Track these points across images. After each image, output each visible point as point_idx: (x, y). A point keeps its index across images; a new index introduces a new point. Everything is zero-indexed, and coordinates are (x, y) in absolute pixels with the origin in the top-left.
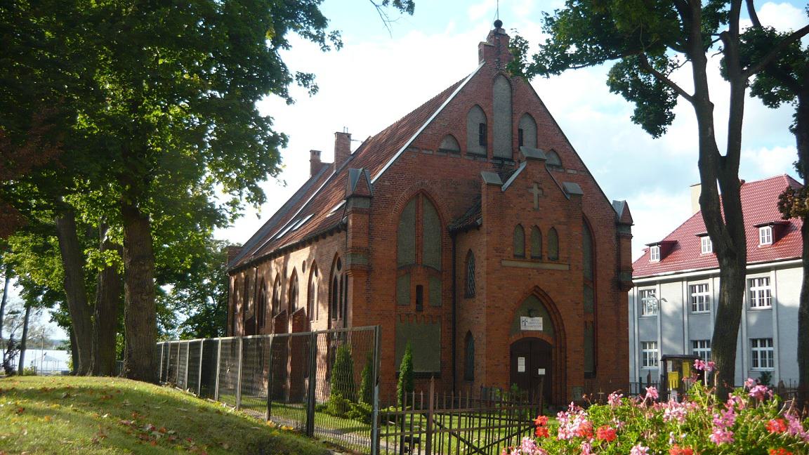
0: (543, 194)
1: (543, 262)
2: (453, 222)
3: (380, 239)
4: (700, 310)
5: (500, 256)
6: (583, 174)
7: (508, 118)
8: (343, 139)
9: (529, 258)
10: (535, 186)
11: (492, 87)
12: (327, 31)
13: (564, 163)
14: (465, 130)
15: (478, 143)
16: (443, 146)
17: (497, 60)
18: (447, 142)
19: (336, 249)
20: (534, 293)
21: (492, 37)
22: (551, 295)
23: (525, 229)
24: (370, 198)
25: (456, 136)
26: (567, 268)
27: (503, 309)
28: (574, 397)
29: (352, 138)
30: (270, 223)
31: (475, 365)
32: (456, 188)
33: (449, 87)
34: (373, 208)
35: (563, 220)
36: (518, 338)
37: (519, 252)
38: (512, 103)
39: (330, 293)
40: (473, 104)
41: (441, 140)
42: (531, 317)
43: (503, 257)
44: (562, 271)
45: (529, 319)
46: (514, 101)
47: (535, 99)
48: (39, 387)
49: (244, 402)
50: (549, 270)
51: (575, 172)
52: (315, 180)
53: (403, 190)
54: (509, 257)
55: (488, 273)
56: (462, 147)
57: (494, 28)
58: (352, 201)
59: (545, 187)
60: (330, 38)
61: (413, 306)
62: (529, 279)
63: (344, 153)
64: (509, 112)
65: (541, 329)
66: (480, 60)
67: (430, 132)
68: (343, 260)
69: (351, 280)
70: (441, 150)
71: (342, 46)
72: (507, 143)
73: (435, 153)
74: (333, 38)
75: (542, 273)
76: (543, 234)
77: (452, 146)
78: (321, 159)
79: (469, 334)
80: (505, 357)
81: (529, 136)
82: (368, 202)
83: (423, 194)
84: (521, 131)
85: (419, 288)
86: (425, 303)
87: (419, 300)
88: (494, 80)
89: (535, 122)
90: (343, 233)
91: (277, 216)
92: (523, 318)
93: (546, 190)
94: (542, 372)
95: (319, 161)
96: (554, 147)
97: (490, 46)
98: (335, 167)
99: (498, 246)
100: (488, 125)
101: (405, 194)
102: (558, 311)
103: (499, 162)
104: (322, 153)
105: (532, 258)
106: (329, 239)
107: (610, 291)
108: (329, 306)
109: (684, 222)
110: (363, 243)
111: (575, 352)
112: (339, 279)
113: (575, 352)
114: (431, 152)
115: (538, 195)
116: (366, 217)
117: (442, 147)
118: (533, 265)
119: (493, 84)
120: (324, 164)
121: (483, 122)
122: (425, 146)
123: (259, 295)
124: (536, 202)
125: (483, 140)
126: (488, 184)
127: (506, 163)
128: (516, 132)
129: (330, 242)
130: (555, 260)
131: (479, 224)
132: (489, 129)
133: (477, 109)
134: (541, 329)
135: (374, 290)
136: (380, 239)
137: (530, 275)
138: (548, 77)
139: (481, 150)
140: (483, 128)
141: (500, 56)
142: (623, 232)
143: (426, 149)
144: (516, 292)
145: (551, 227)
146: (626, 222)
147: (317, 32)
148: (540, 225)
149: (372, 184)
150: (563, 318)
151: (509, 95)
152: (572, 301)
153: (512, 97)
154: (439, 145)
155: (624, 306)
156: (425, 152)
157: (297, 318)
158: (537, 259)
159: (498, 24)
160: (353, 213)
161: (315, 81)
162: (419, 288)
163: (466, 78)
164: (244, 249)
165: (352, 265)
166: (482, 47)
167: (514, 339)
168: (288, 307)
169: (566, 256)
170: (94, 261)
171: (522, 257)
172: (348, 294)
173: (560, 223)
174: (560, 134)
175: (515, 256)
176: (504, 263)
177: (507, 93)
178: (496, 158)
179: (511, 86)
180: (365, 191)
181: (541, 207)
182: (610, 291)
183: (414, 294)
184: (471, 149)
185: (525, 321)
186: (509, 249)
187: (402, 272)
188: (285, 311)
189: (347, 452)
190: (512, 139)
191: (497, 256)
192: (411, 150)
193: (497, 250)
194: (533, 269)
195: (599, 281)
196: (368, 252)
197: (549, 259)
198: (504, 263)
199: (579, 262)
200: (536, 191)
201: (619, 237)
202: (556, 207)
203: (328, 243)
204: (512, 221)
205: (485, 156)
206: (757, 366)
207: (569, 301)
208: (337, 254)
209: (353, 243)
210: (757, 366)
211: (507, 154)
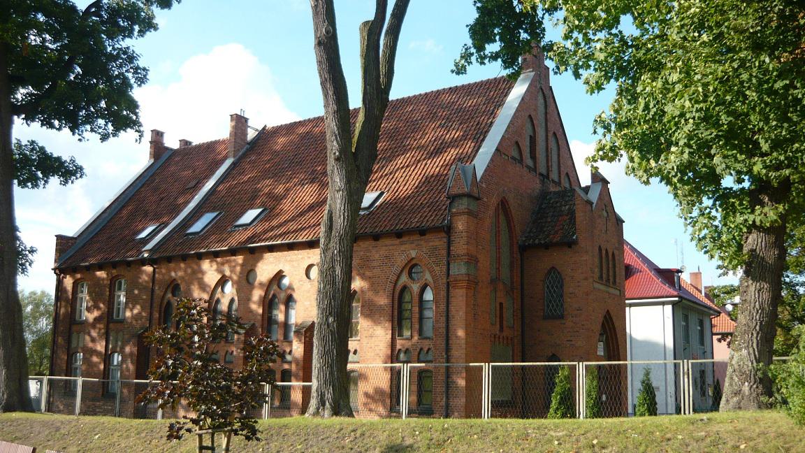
8: (240, 122)
30: (113, 206)
33: (288, 123)
48: (657, 399)
49: (672, 408)
63: (242, 140)
78: (165, 141)
91: (123, 196)
95: (162, 144)
104: (165, 136)
108: (392, 321)
120: (167, 149)
164: (78, 241)
168: (102, 373)
170: (631, 40)
206: (479, 415)
210: (479, 415)
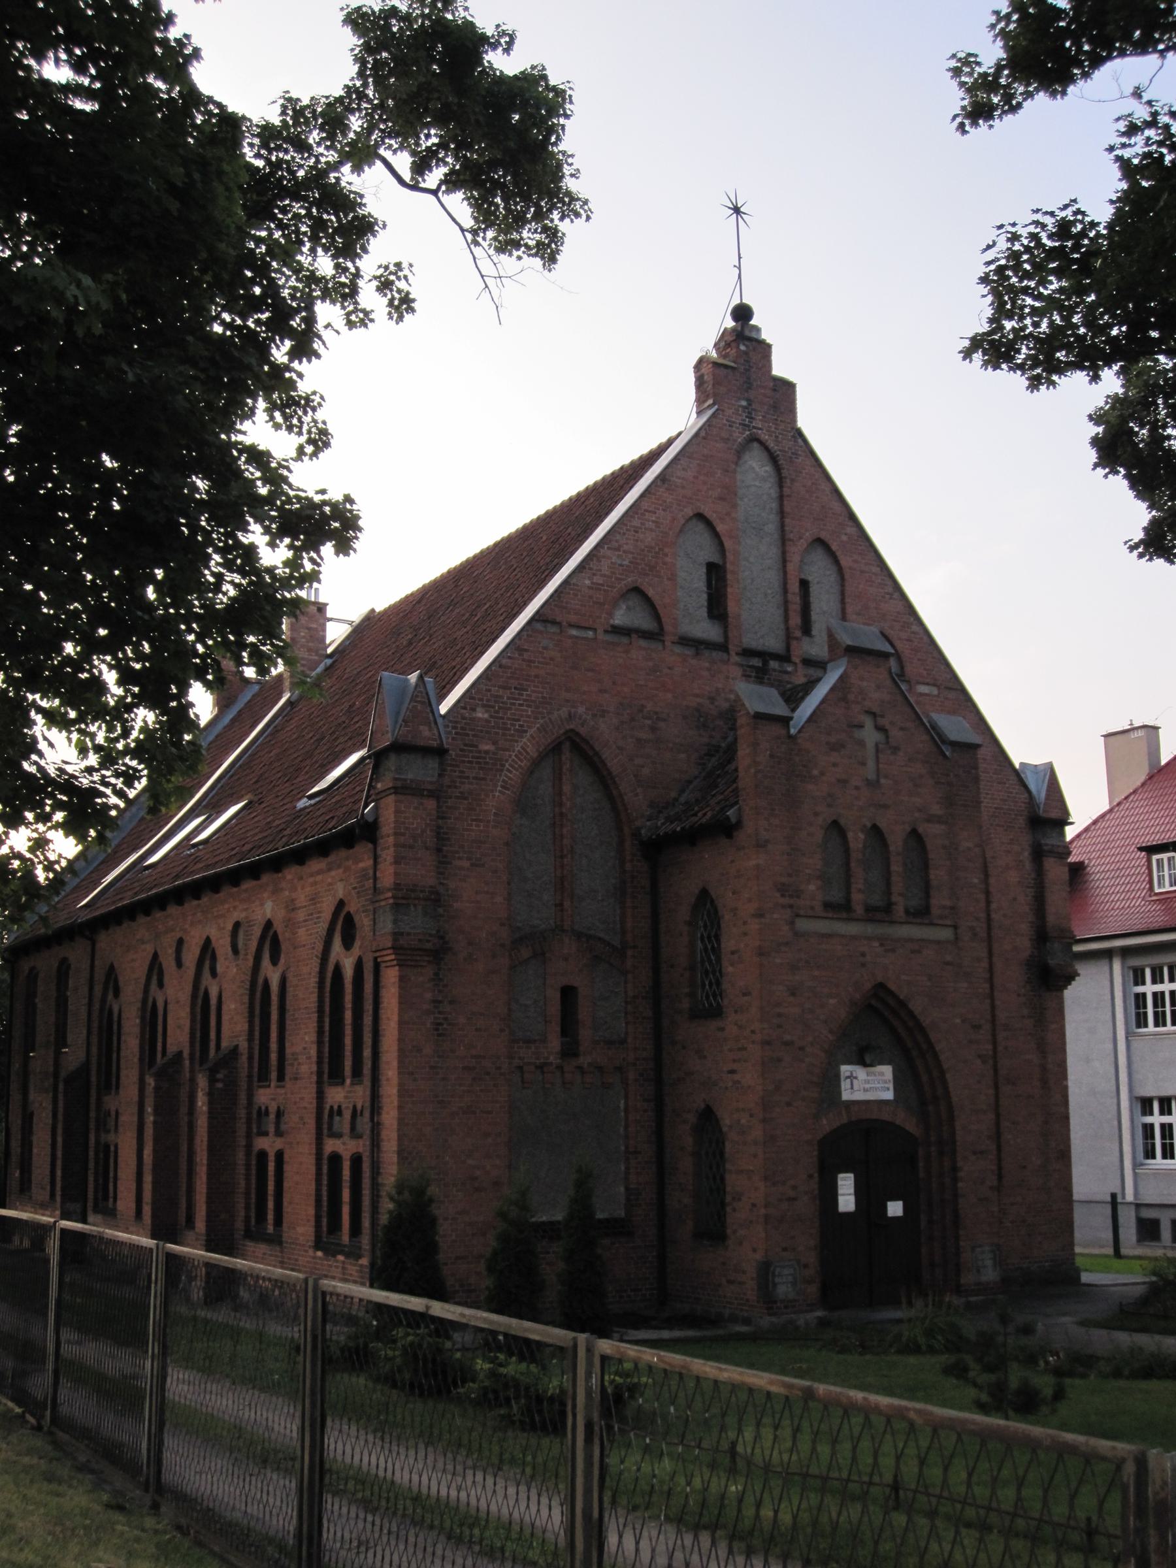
0: (888, 743)
1: (892, 922)
2: (650, 819)
3: (466, 864)
4: (1157, 1025)
5: (791, 906)
6: (952, 695)
7: (774, 552)
9: (859, 910)
10: (869, 723)
11: (735, 472)
12: (369, 264)
13: (908, 669)
14: (673, 578)
15: (704, 612)
16: (620, 617)
17: (744, 403)
18: (628, 608)
19: (340, 891)
20: (873, 1002)
21: (728, 345)
22: (916, 1006)
23: (850, 835)
24: (440, 752)
25: (650, 593)
26: (945, 934)
27: (802, 1049)
28: (978, 1271)
29: (329, 614)
31: (728, 1199)
32: (653, 729)
34: (446, 781)
35: (936, 810)
36: (837, 1124)
37: (837, 896)
38: (782, 513)
39: (320, 1011)
40: (689, 512)
41: (615, 604)
42: (864, 1064)
44: (938, 942)
45: (860, 1072)
46: (787, 509)
47: (836, 506)
50: (911, 940)
51: (935, 691)
52: (226, 720)
53: (522, 732)
54: (812, 908)
55: (761, 952)
56: (668, 628)
57: (730, 323)
58: (392, 762)
59: (892, 723)
60: (375, 283)
61: (555, 1043)
62: (863, 965)
63: (310, 650)
64: (776, 536)
65: (889, 1095)
66: (700, 400)
67: (587, 582)
68: (363, 922)
69: (391, 976)
70: (616, 630)
71: (411, 310)
72: (773, 613)
73: (601, 636)
74: (385, 285)
75: (893, 950)
76: (892, 848)
77: (640, 619)
79: (708, 1116)
80: (811, 1176)
81: (824, 603)
82: (433, 764)
83: (573, 743)
84: (804, 584)
86: (585, 1034)
87: (568, 1024)
88: (740, 453)
89: (836, 561)
90: (363, 850)
92: (845, 1069)
93: (894, 733)
94: (895, 1209)
97: (726, 367)
98: (287, 684)
100: (728, 566)
101: (527, 745)
102: (931, 1046)
103: (756, 662)
106: (316, 864)
109: (1094, 818)
110: (422, 873)
112: (348, 972)
113: (975, 1153)
114: (590, 634)
115: (877, 745)
116: (431, 804)
118: (870, 929)
119: (736, 464)
121: (715, 558)
122: (573, 618)
123: (102, 1010)
124: (871, 764)
125: (717, 607)
126: (759, 716)
127: (773, 664)
128: (794, 587)
129: (319, 872)
130: (921, 914)
131: (733, 820)
132: (729, 576)
133: (700, 527)
134: (889, 1095)
135: (451, 1002)
136: (466, 864)
137: (863, 955)
138: (1053, 383)
139: (707, 630)
140: (716, 574)
142: (1049, 841)
143: (579, 627)
144: (832, 1001)
145: (908, 829)
146: (1054, 814)
147: (337, 266)
148: (883, 824)
149: (443, 717)
150: (945, 1066)
151: (774, 493)
152: (963, 1021)
153: (781, 497)
154: (611, 615)
155: (1054, 1026)
156: (574, 632)
157: (220, 1076)
158: (880, 912)
159: (742, 313)
160: (395, 793)
161: (320, 415)
162: (568, 994)
163: (670, 442)
165: (396, 935)
166: (706, 369)
167: (827, 1124)
169: (948, 903)
171: (840, 908)
172: (383, 1014)
173: (930, 819)
174: (896, 595)
176: (803, 925)
177: (769, 488)
178: (748, 653)
179: (778, 468)
180: (426, 736)
181: (886, 777)
183: (554, 1008)
185: (851, 1077)
186: (812, 887)
187: (525, 953)
188: (180, 1053)
189: (491, 1553)
190: (786, 602)
191: (783, 907)
192: (539, 626)
193: (783, 889)
194: (869, 939)
196: (435, 900)
197: (907, 912)
198: (803, 925)
199: (977, 919)
200: (870, 735)
203: (312, 875)
204: (816, 814)
205: (723, 647)
207: (958, 1021)
208: (341, 904)
209: (396, 874)
211: (773, 643)
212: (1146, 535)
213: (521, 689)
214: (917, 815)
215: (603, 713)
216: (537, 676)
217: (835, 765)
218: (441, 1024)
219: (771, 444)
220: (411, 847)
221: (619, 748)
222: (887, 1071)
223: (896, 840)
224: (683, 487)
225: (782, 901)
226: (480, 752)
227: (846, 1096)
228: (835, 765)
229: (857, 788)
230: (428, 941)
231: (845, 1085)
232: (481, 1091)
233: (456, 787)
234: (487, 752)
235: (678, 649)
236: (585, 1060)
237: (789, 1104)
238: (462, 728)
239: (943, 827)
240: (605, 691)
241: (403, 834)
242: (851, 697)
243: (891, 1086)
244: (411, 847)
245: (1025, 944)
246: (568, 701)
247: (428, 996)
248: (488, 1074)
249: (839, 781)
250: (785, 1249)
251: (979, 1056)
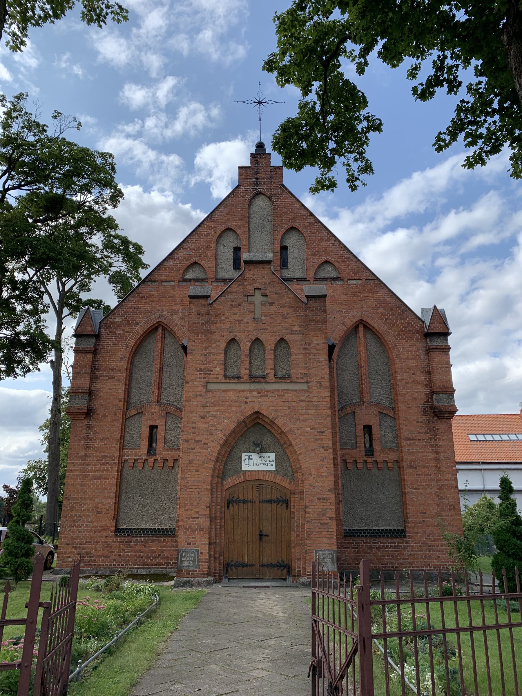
3: (106, 378)
9: (246, 378)
15: (232, 267)
22: (279, 422)
23: (242, 344)
35: (297, 328)
43: (209, 378)
45: (255, 456)
51: (360, 282)
54: (217, 378)
59: (271, 292)
62: (246, 403)
65: (273, 468)
67: (171, 263)
75: (267, 396)
82: (92, 341)
85: (153, 428)
86: (159, 446)
92: (245, 455)
96: (330, 259)
99: (203, 367)
105: (251, 377)
107: (420, 420)
111: (319, 498)
113: (319, 498)
114: (172, 283)
117: (187, 277)
118: (253, 386)
122: (164, 278)
130: (285, 379)
137: (247, 398)
141: (259, 175)
144: (225, 421)
156: (164, 284)
162: (153, 428)
169: (303, 371)
173: (292, 333)
175: (225, 377)
182: (420, 420)
184: (222, 275)
186: (218, 369)
191: (200, 378)
193: (200, 371)
194: (253, 390)
195: (402, 407)
200: (258, 298)
201: (429, 351)
202: (288, 314)
207: (308, 429)
212: (411, 174)
213: (138, 308)
214: (285, 331)
215: (176, 313)
216: (145, 302)
217: (235, 314)
218: (88, 443)
219: (268, 193)
220: (80, 373)
221: (182, 326)
222: (272, 456)
223: (270, 343)
224: (220, 219)
225: (201, 376)
226: (116, 334)
227: (244, 468)
228: (235, 314)
229: (247, 323)
230: (82, 409)
231: (244, 463)
232: (104, 470)
233: (104, 348)
234: (120, 334)
235: (214, 284)
236: (158, 457)
237: (197, 471)
238: (109, 326)
239: (300, 336)
240: (178, 304)
241: (77, 368)
242: (246, 283)
243: (274, 463)
244: (80, 373)
245: (422, 398)
246: (159, 310)
247: (84, 431)
248: (108, 463)
249: (237, 321)
250: (189, 544)
251: (323, 447)
